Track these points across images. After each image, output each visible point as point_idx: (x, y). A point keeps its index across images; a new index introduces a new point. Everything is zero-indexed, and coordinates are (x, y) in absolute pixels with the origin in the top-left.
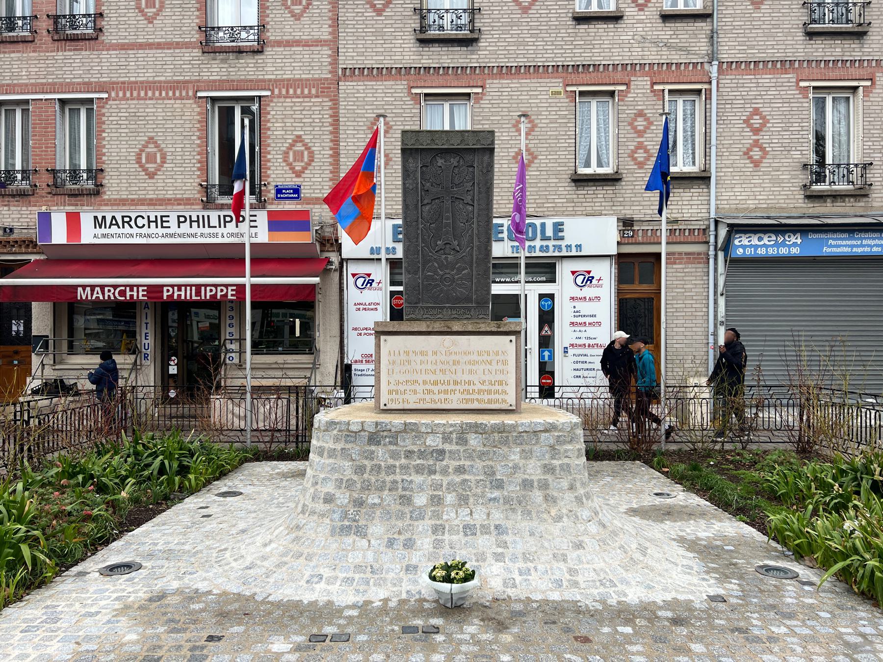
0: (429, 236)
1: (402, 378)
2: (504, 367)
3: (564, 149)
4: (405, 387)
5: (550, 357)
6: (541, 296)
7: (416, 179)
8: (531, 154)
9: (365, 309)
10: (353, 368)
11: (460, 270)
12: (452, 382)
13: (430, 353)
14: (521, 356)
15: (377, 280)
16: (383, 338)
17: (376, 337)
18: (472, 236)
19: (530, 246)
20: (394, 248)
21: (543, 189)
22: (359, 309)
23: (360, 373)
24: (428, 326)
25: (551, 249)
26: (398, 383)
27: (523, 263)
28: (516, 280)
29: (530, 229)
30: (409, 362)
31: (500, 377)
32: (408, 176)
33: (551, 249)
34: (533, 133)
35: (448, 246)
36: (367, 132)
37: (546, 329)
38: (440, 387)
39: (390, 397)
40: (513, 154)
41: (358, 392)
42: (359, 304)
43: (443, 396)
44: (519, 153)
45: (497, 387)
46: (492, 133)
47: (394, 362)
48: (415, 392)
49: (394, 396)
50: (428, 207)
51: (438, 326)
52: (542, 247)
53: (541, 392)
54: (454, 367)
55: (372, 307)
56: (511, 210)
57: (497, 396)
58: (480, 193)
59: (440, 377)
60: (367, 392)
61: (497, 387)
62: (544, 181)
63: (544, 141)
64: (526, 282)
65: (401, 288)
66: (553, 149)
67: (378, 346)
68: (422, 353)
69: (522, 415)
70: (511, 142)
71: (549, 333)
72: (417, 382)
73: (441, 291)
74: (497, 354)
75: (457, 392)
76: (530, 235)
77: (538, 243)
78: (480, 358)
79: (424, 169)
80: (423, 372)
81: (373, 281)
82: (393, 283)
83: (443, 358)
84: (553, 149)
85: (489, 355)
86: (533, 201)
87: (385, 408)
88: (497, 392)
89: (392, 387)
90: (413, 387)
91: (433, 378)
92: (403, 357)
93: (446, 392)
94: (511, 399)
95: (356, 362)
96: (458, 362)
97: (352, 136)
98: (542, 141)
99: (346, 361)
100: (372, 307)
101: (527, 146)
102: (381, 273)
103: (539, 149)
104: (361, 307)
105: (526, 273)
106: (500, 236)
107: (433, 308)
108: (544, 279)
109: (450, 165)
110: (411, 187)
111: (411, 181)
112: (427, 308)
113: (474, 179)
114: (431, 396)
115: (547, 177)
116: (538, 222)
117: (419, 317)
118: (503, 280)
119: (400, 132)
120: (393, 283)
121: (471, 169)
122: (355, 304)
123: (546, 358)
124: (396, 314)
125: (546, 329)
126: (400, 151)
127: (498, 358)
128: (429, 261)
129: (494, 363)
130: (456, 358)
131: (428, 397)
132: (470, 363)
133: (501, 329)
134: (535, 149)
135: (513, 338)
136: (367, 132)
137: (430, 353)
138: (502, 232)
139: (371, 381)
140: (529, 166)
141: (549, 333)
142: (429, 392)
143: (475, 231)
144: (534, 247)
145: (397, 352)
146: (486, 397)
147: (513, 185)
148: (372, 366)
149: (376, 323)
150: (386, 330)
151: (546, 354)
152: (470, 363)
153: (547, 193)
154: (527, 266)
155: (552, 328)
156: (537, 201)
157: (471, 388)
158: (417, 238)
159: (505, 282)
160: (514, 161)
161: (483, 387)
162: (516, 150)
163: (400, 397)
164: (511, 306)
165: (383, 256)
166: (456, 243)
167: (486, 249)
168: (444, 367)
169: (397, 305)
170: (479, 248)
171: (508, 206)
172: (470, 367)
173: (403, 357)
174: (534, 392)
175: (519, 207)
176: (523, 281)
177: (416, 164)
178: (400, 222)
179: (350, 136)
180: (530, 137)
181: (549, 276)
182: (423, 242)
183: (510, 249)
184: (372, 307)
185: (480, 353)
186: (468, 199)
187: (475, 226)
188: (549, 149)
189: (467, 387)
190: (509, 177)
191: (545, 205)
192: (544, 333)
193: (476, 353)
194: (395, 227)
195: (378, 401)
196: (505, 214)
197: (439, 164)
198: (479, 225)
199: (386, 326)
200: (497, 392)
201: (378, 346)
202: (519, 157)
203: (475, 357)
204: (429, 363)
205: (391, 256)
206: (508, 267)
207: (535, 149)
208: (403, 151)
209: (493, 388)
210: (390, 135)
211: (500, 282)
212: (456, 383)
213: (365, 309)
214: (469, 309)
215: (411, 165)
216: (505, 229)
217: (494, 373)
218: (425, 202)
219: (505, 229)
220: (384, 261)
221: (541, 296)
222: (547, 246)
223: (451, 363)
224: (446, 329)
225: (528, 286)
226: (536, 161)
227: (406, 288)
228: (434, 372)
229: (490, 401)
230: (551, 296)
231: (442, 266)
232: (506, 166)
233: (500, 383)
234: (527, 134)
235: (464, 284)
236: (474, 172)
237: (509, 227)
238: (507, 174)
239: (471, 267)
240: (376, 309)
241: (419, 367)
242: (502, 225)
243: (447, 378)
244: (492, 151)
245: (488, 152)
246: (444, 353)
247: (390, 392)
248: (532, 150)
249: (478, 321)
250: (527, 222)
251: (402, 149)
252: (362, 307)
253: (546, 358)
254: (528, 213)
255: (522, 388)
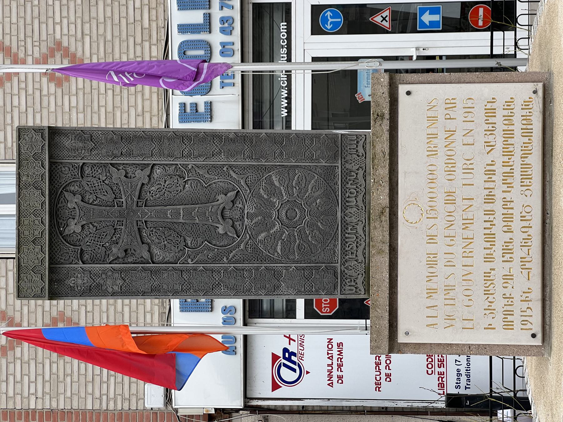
0: (209, 249)
1: (480, 301)
2: (459, 105)
3: (65, 9)
4: (498, 296)
5: (434, 11)
6: (316, 30)
7: (104, 272)
8: (52, 53)
9: (340, 366)
10: (455, 391)
11: (273, 191)
12: (489, 207)
13: (432, 248)
14: (431, 69)
15: (285, 343)
16: (402, 339)
17: (399, 352)
18: (211, 169)
19: (222, 53)
20: (225, 310)
21: (116, 29)
22: (340, 378)
23: (464, 379)
24: (380, 252)
25: (227, 12)
26: (490, 310)
27: (252, 67)
28: (284, 77)
29: (191, 53)
30: (449, 289)
31: (479, 114)
32: (99, 286)
33: (227, 12)
34: (14, 50)
35: (227, 213)
36: (10, 359)
37: (378, 19)
38: (498, 229)
39: (517, 325)
40: (52, 86)
41: (503, 385)
42: (330, 376)
43: (516, 225)
44: (51, 76)
45: (499, 120)
46: (21, 132)
47: (449, 318)
48: (508, 278)
49: (516, 318)
50: (155, 250)
51: (380, 233)
52: (223, 31)
53: (503, 29)
54: (459, 201)
55: (336, 355)
56: (155, 89)
57: (517, 120)
58: (130, 154)
59: (478, 230)
60: (503, 367)
61: (499, 120)
62: (101, 27)
63: (29, 28)
64: (289, 60)
65: (300, 304)
66: (43, 10)
67: (416, 348)
68: (432, 264)
69: (555, 70)
70: (30, 91)
71: (386, 13)
72: (487, 275)
73: (311, 225)
74: (433, 119)
75: (508, 196)
76: (201, 52)
77: (216, 38)
78: (442, 152)
79: (86, 257)
80: (468, 261)
81: (285, 350)
82: (290, 313)
83: (441, 223)
84: (43, 10)
85: (433, 136)
86: (138, 48)
87: (539, 336)
88: (508, 119)
89: (498, 322)
90: (498, 282)
91: (479, 245)
92: (439, 299)
93: (507, 218)
94: (521, 93)
95: (441, 385)
96: (449, 193)
97: (18, 386)
98: (29, 33)
99: (442, 405)
100: (336, 355)
101: (37, 62)
102: (270, 337)
103: (44, 37)
104: (335, 373)
105: (272, 60)
106: (202, 109)
107: (344, 243)
108: (283, 25)
109: (81, 209)
110: (120, 282)
111: (109, 282)
112: (344, 253)
113: (105, 165)
114: (516, 246)
115: (94, 22)
116: (177, 39)
117: (361, 268)
118: (284, 103)
119: (18, 302)
120: (290, 313)
121: (87, 170)
122: (331, 385)
123: (436, 18)
124: (353, 309)
125: (378, 19)
126: (54, 302)
127: (441, 118)
128: (255, 249)
129: (451, 125)
130: (441, 198)
131: (518, 253)
132: (450, 172)
133: (386, 111)
134: (44, 45)
135: (402, 89)
136: (10, 359)
137: (432, 248)
138: (195, 106)
139: (480, 363)
140: (74, 56)
141: (386, 13)
142: (507, 250)
143: (200, 162)
144: (223, 45)
145: (430, 312)
146: (518, 140)
147: (109, 85)
148: (451, 359)
149: (373, 350)
150: (386, 332)
151: (427, 18)
152: (450, 172)
153: (124, 21)
154: (258, 58)
155: (375, 9)
156: (139, 40)
157: (499, 169)
158: (213, 271)
159: (289, 98)
160: (65, 84)
161: (499, 145)
162: (45, 80)
163: (518, 306)
164: (335, 90)
165: (239, 331)
166: (221, 198)
167: (233, 141)
168: (459, 222)
169: (332, 307)
170: (231, 154)
171: (147, 95)
172: (459, 170)
173: (439, 299)
174: (503, 41)
175: (147, 74)
176: (288, 67)
177: (77, 273)
178: (176, 303)
179: (18, 390)
180: (21, 55)
181: (277, 16)
182: (220, 261)
183: (228, 89)
184: (335, 352)
185: (432, 153)
186: (141, 176)
187: (191, 163)
188: (43, 19)
189: (498, 178)
190: (95, 93)
191: (146, 25)
192: (386, 24)
193: (433, 160)
194: (183, 309)
195: (527, 350)
196: (162, 101)
197: (78, 229)
198: (189, 156)
199: (379, 332)
200: (508, 119)
201: (416, 348)
202: (57, 74)
203: (440, 161)
204: (450, 249)
205: (239, 315)
206: (261, 98)
207: (44, 45)
208: (53, 295)
209: (500, 126)
210: (18, 315)
211: (289, 108)
212: (490, 199)
213: (340, 366)
214: (346, 173)
215: (78, 281)
216: (189, 100)
217: (470, 126)
218: (146, 255)
219: (189, 100)
220: (247, 331)
221: (316, 30)
222: (223, 20)
223: (451, 208)
224: (386, 218)
225: (297, 56)
226: (65, 44)
227: (299, 294)
228: (469, 240)
229: (527, 133)
230: (316, 10)
231: (265, 225)
232: (74, 99)
233: (490, 112)
234: (15, 61)
235: (298, 183)
236: (93, 165)
237: (186, 94)
238: (88, 97)
239: (267, 169)
240: (340, 345)
241: (459, 271)
242: (183, 106)
243: (480, 216)
244: (54, 132)
245: (57, 139)
246: (432, 222)
247: (508, 326)
248: (44, 50)
249: (370, 155)
250: (176, 57)
251: (51, 298)
252: (335, 375)
253: (436, 18)
254: (161, 57)
255: (498, 68)
